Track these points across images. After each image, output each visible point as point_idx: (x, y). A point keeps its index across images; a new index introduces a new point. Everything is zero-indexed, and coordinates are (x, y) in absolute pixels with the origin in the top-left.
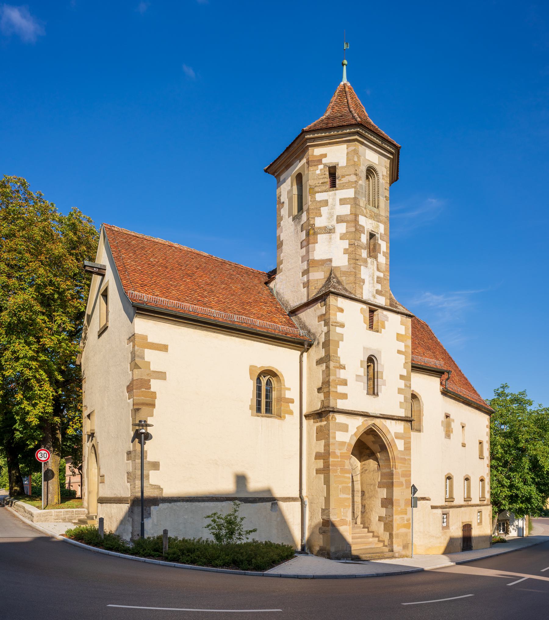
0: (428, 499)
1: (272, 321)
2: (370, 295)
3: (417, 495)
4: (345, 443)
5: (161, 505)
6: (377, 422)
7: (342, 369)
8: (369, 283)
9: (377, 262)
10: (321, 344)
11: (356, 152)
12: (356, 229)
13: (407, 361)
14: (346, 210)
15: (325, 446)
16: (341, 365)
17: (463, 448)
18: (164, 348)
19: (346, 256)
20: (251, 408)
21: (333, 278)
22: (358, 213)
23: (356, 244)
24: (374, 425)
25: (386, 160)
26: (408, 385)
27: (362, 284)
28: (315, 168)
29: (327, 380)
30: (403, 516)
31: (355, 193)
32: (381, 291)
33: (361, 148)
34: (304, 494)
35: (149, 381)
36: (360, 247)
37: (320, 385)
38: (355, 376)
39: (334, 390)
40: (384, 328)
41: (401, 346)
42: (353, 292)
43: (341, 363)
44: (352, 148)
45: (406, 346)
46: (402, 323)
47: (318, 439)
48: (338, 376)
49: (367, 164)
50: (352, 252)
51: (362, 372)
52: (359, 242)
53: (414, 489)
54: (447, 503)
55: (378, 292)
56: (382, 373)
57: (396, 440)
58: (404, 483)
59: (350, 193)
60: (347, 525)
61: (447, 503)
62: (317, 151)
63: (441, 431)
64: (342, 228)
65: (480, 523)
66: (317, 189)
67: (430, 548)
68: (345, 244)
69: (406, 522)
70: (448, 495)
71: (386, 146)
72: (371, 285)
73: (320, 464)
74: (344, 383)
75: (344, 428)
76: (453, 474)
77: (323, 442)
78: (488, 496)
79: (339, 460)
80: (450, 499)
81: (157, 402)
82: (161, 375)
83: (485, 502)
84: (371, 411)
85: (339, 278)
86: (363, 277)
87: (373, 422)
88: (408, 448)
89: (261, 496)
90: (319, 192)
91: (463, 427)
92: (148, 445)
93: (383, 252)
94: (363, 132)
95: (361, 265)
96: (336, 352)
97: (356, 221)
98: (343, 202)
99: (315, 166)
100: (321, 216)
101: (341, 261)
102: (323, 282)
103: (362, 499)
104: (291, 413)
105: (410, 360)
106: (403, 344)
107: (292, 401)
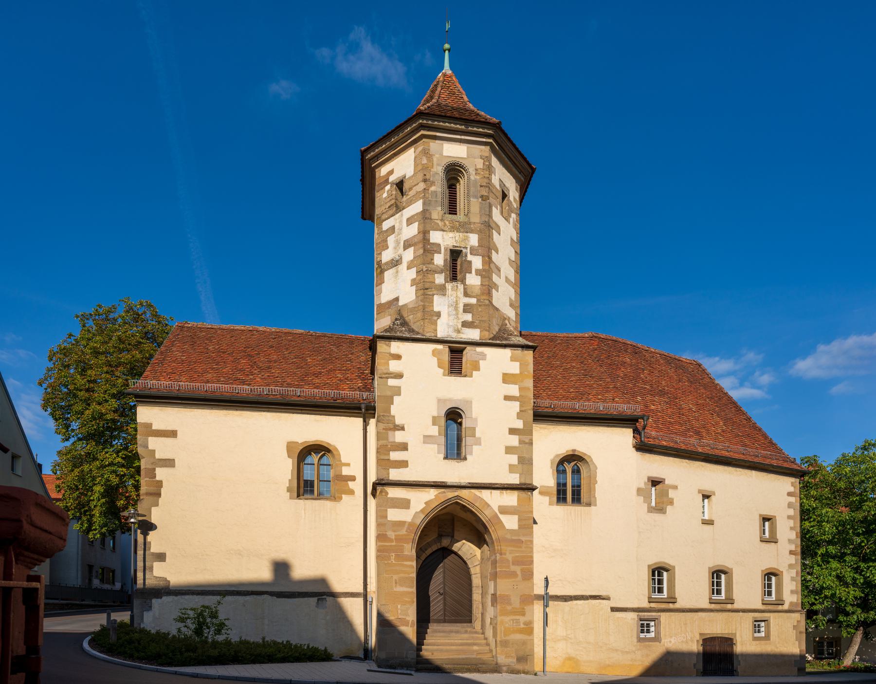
0: (607, 598)
2: (451, 330)
4: (405, 522)
5: (164, 598)
6: (464, 493)
7: (399, 430)
8: (449, 315)
12: (425, 251)
16: (398, 426)
18: (173, 434)
20: (289, 490)
22: (428, 229)
25: (483, 147)
30: (517, 617)
31: (424, 204)
32: (472, 322)
33: (434, 145)
34: (372, 586)
35: (154, 469)
36: (478, 272)
39: (386, 457)
42: (421, 331)
44: (420, 149)
46: (513, 359)
48: (391, 440)
49: (445, 162)
52: (431, 266)
55: (465, 324)
57: (501, 517)
62: (383, 171)
67: (609, 666)
68: (413, 274)
69: (522, 626)
71: (475, 129)
72: (452, 317)
79: (394, 544)
81: (163, 491)
82: (169, 463)
84: (450, 480)
87: (456, 494)
89: (304, 590)
92: (152, 536)
93: (477, 271)
94: (430, 122)
95: (433, 295)
96: (388, 410)
98: (410, 221)
106: (517, 386)
107: (353, 479)
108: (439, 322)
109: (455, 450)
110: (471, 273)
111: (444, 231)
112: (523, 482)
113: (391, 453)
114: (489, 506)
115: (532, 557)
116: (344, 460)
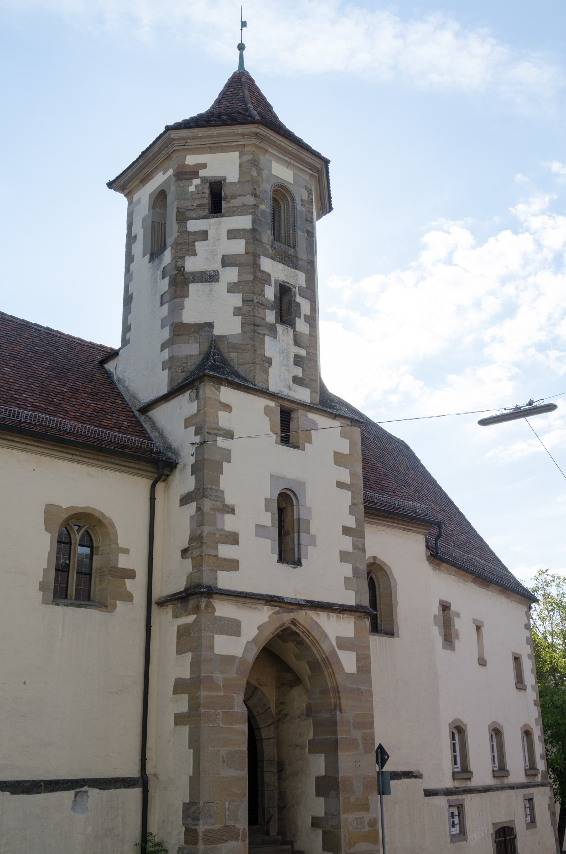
1: (100, 426)
3: (389, 767)
4: (233, 658)
6: (302, 616)
7: (228, 512)
9: (295, 331)
10: (189, 468)
11: (255, 163)
12: (255, 277)
13: (355, 502)
14: (238, 247)
15: (193, 664)
16: (227, 506)
17: (482, 669)
19: (239, 319)
20: (43, 587)
21: (215, 354)
23: (255, 301)
24: (293, 622)
26: (360, 546)
27: (267, 365)
28: (187, 183)
29: (198, 533)
31: (254, 222)
32: (302, 379)
36: (263, 305)
37: (185, 544)
38: (254, 527)
39: (213, 552)
40: (310, 442)
41: (345, 476)
43: (226, 503)
45: (352, 475)
46: (343, 435)
47: (180, 651)
50: (249, 313)
51: (268, 519)
52: (262, 298)
53: (382, 755)
54: (458, 784)
56: (308, 522)
57: (339, 652)
58: (360, 742)
59: (244, 222)
60: (237, 839)
61: (458, 784)
63: (436, 634)
64: (230, 275)
65: (532, 823)
66: (189, 214)
68: (237, 300)
70: (497, 764)
73: (182, 705)
74: (233, 539)
75: (233, 628)
76: (501, 723)
77: (189, 656)
78: (541, 765)
79: (221, 694)
80: (463, 771)
83: (539, 779)
84: (287, 593)
85: (226, 355)
86: (268, 354)
88: (364, 666)
90: (192, 219)
91: (478, 628)
93: (305, 316)
95: (264, 335)
96: (216, 482)
97: (256, 265)
98: (233, 234)
99: (187, 179)
100: (196, 255)
101: (228, 326)
102: (198, 360)
103: (279, 778)
104: (128, 598)
105: (361, 500)
106: (347, 472)
107: (131, 574)
108: (271, 370)
109: (288, 552)
110: (300, 317)
111: (274, 260)
112: (359, 603)
113: (220, 546)
114: (326, 636)
115: (372, 716)
116: (122, 542)
